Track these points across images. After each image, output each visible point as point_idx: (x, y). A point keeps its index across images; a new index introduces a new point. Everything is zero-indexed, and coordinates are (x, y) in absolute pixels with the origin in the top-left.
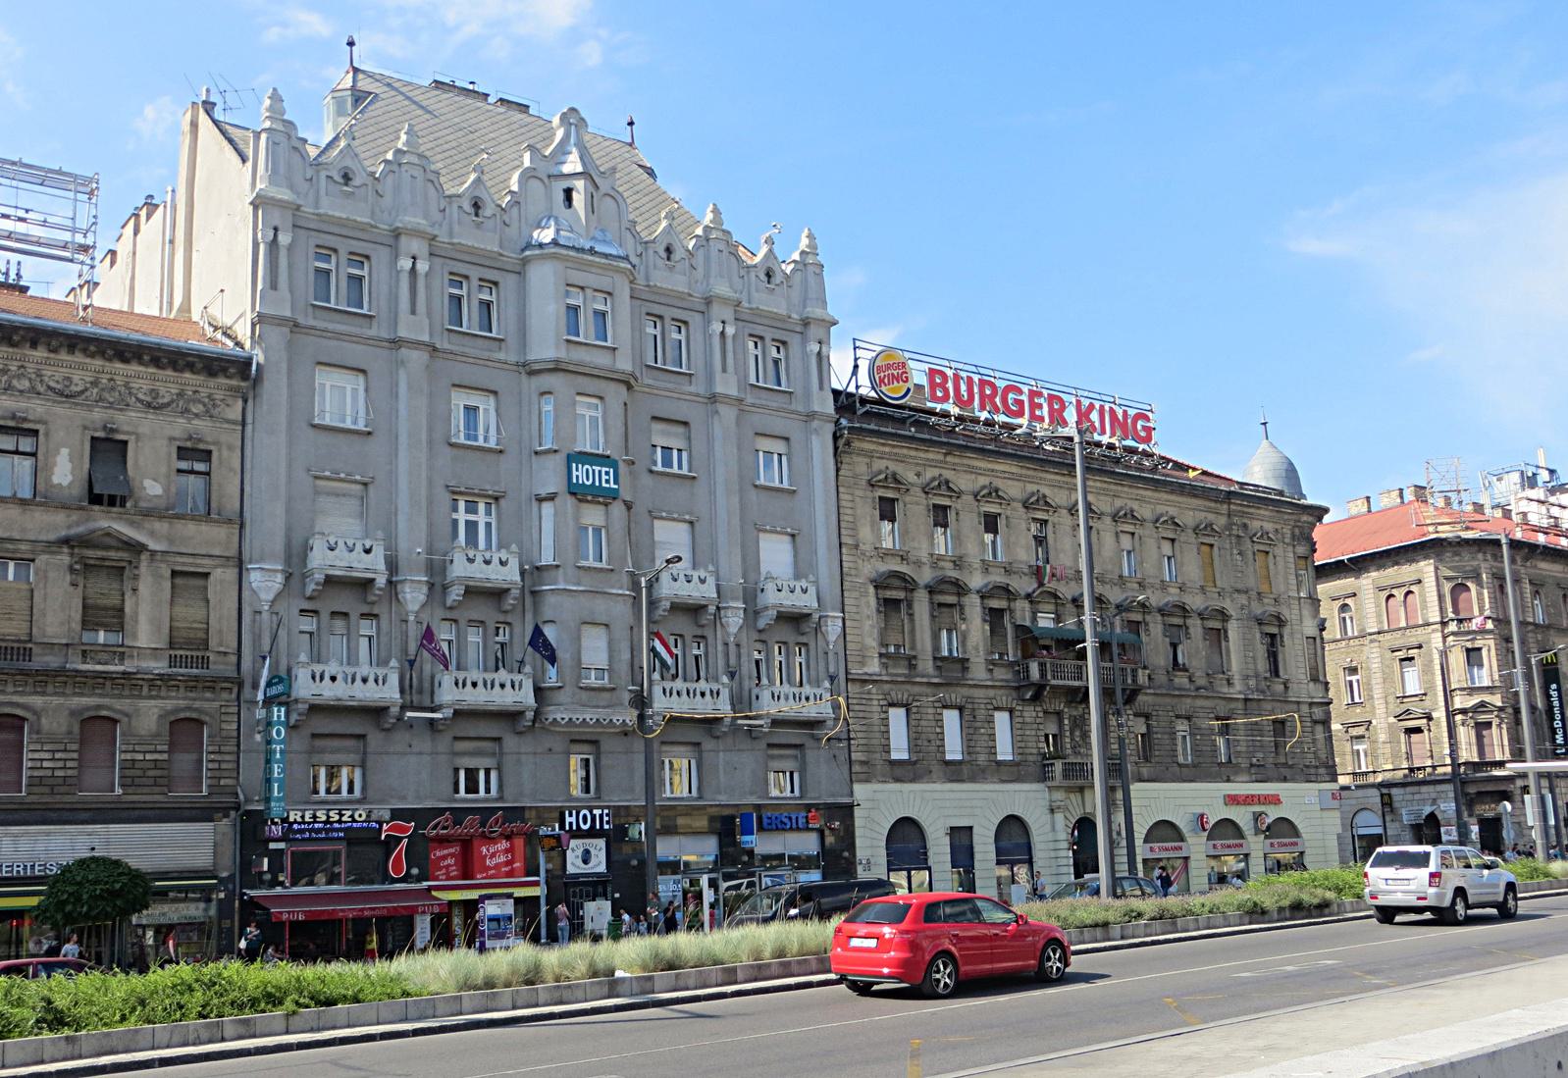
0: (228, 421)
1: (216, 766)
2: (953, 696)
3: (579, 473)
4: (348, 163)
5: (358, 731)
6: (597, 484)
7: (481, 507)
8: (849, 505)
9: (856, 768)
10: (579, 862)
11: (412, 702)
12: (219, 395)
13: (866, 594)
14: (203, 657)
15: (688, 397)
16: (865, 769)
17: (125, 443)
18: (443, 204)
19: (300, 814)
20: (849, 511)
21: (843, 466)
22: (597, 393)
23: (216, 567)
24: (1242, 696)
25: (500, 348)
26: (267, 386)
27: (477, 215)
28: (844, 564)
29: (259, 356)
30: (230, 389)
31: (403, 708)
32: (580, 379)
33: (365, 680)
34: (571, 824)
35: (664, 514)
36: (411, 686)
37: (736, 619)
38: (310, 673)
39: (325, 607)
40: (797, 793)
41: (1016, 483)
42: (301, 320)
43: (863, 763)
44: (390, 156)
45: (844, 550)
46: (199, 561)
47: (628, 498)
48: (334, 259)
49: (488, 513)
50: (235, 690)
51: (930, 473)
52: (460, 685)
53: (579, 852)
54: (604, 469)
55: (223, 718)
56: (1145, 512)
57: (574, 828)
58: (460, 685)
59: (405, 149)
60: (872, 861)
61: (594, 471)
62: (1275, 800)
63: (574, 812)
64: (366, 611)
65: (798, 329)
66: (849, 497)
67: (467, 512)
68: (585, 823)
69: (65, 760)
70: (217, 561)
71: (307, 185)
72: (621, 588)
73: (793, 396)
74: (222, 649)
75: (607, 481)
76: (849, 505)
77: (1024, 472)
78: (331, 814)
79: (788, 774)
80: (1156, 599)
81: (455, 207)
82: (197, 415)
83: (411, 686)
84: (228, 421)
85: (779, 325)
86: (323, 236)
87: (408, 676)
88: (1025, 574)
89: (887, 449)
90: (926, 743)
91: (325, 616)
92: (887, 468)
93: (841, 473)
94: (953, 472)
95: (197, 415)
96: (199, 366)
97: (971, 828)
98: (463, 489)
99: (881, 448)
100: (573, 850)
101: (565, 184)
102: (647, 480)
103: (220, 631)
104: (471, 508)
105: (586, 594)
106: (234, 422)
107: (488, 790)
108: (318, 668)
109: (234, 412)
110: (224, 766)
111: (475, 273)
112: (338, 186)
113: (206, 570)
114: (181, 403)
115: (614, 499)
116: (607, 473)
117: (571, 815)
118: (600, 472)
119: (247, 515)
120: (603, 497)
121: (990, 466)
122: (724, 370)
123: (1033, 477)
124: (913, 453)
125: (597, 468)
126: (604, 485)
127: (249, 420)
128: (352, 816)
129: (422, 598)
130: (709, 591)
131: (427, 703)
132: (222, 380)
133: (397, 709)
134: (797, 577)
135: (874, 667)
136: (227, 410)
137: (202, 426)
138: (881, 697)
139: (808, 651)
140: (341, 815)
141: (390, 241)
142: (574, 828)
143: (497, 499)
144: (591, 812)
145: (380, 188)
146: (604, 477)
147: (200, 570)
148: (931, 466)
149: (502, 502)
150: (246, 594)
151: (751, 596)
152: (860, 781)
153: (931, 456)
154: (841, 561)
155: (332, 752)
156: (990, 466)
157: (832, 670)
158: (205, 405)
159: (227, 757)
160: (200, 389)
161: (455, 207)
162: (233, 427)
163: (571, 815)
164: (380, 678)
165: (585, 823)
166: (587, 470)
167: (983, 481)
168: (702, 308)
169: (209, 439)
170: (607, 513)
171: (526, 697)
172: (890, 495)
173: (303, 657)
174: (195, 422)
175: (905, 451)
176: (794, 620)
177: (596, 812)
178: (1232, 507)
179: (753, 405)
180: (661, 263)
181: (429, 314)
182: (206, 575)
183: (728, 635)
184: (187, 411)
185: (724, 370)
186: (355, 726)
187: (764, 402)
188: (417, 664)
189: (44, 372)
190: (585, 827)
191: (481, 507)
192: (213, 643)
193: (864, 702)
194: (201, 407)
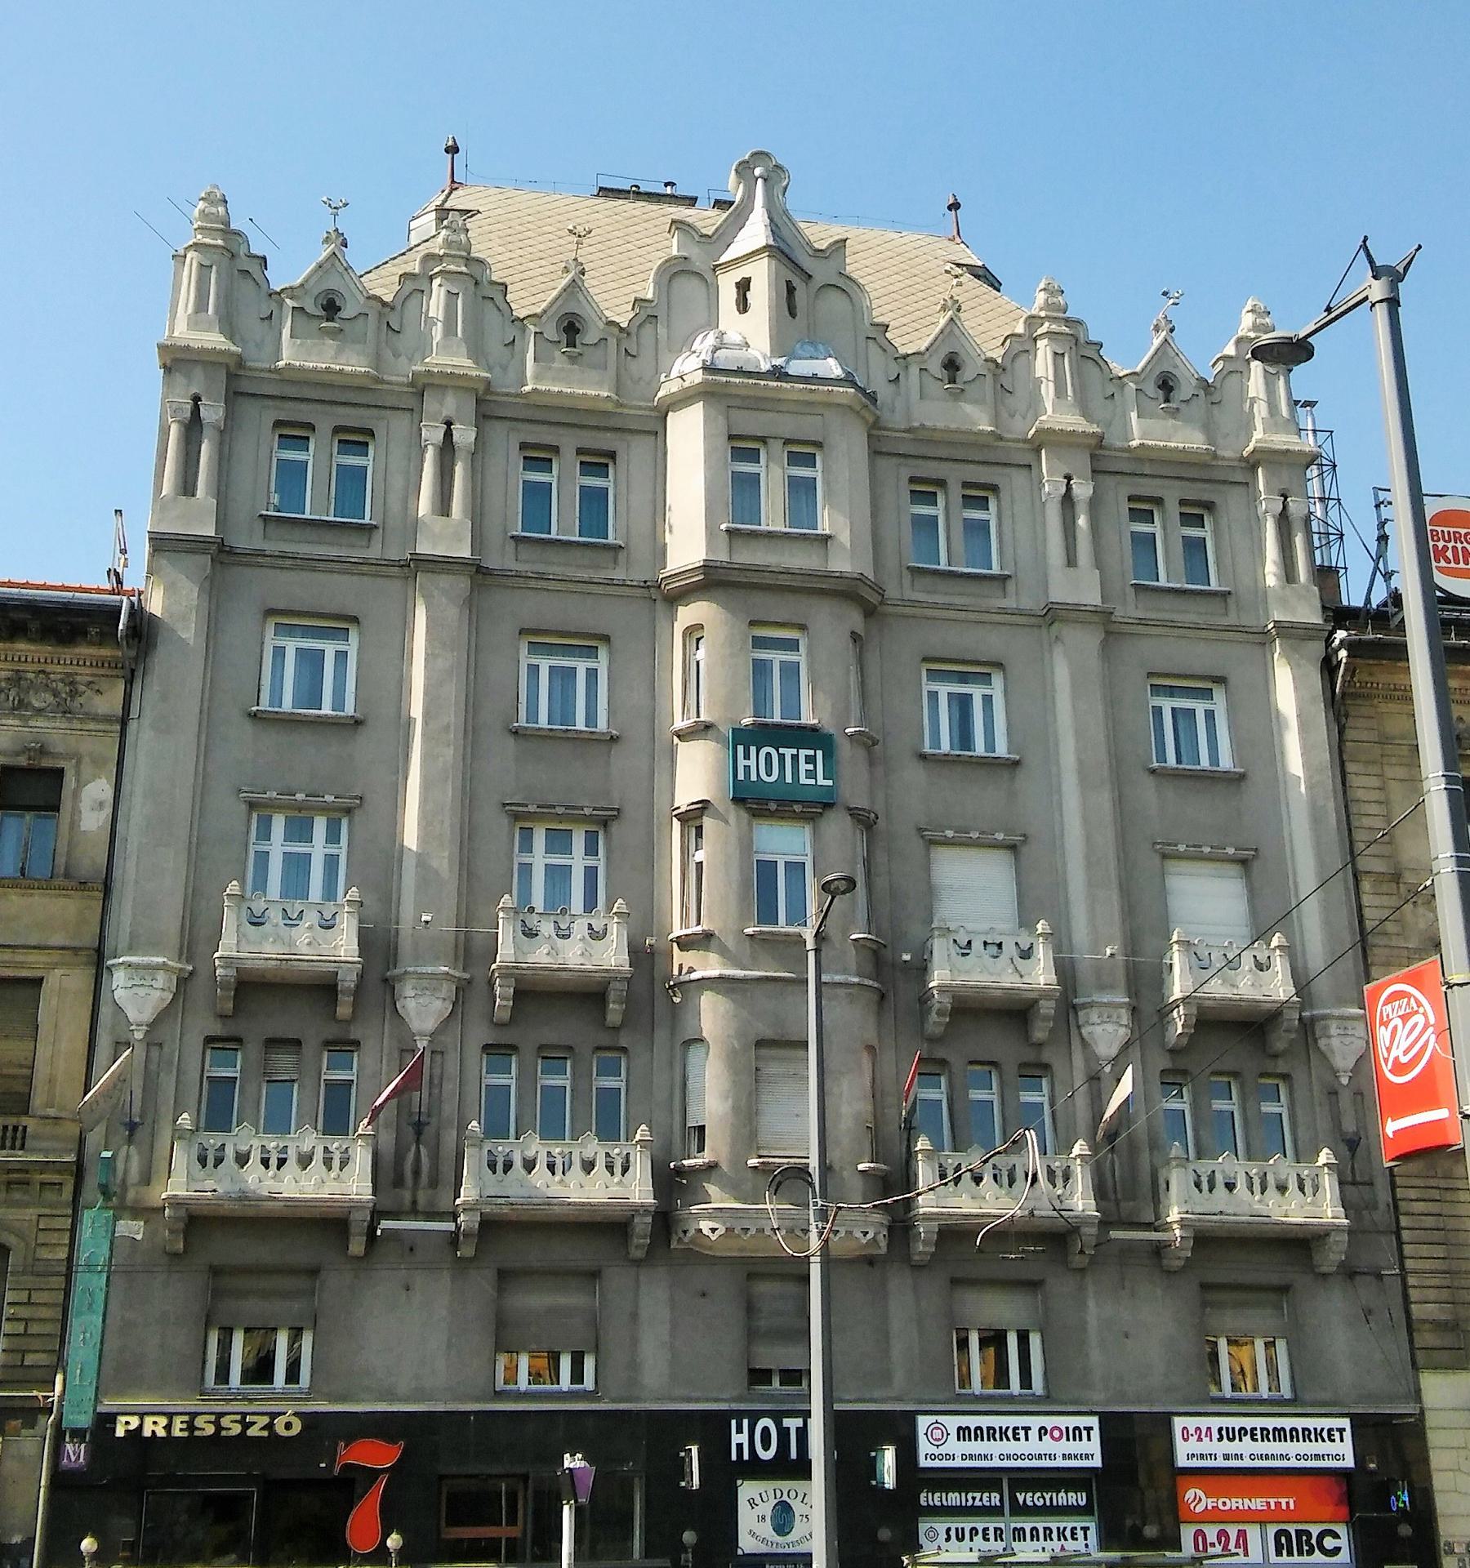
0: (95, 718)
1: (21, 1329)
3: (752, 763)
4: (333, 283)
5: (1274, 1279)
6: (789, 779)
7: (320, 826)
8: (1375, 795)
9: (1426, 1338)
10: (767, 1530)
11: (414, 1203)
12: (84, 674)
14: (15, 1129)
15: (998, 618)
16: (1448, 1340)
17: (59, 773)
18: (511, 332)
19: (163, 1421)
20: (1374, 809)
21: (1351, 722)
22: (795, 620)
23: (54, 966)
25: (615, 561)
26: (162, 659)
27: (571, 344)
28: (1367, 912)
29: (155, 605)
30: (101, 663)
31: (1105, 1224)
32: (758, 598)
33: (1282, 1188)
34: (740, 1446)
35: (950, 833)
36: (417, 1173)
37: (1110, 1028)
38: (1192, 1178)
39: (257, 1029)
40: (589, 1383)
42: (492, 562)
43: (1438, 1326)
44: (1230, 350)
45: (1366, 885)
46: (19, 958)
47: (861, 802)
48: (992, 505)
49: (333, 837)
50: (68, 1189)
52: (1205, 1186)
53: (767, 1509)
54: (803, 753)
55: (42, 1238)
57: (746, 1457)
58: (1205, 1186)
59: (1043, 314)
61: (782, 757)
63: (746, 1422)
64: (606, 1042)
65: (1239, 478)
66: (1374, 782)
67: (288, 838)
68: (766, 1446)
69: (27, 1321)
70: (56, 956)
71: (892, 387)
72: (845, 971)
73: (1231, 601)
74: (51, 1112)
75: (811, 774)
76: (1375, 795)
78: (225, 1422)
79: (1012, 1341)
81: (914, 370)
82: (39, 712)
83: (417, 1173)
84: (95, 718)
86: (341, 410)
87: (411, 1156)
91: (254, 1048)
93: (1350, 734)
95: (39, 712)
96: (34, 626)
98: (532, 808)
100: (752, 1503)
101: (737, 275)
102: (913, 775)
103: (51, 1081)
104: (300, 830)
105: (770, 986)
106: (107, 719)
107: (1026, 1381)
108: (213, 1140)
109: (110, 701)
110: (34, 1329)
111: (569, 442)
112: (315, 324)
113: (38, 974)
114: (12, 693)
115: (828, 806)
116: (811, 760)
117: (740, 1430)
118: (795, 758)
119: (117, 873)
120: (808, 808)
122: (1071, 561)
125: (789, 752)
126: (803, 780)
127: (134, 714)
128: (270, 1427)
129: (1123, 1033)
130: (1041, 974)
131: (1148, 1217)
132: (84, 651)
133: (1094, 1231)
134: (1026, 922)
136: (98, 699)
137: (53, 731)
139: (1291, 1093)
140: (246, 1426)
141: (411, 402)
142: (746, 1457)
143: (348, 811)
144: (779, 1425)
145: (1006, 381)
146: (803, 767)
147: (24, 973)
149: (615, 827)
150: (105, 1011)
151: (1143, 982)
152: (1434, 1368)
154: (1360, 908)
155: (265, 1295)
157: (1349, 1126)
158: (56, 694)
159: (44, 1313)
160: (49, 668)
161: (914, 370)
162: (108, 728)
163: (740, 1430)
164: (1204, 1179)
165: (766, 1446)
166: (768, 755)
168: (411, 402)
169: (60, 749)
170: (816, 834)
171: (638, 1189)
173: (185, 1120)
174: (40, 722)
176: (1247, 1027)
177: (787, 1422)
179: (1142, 622)
180: (936, 389)
181: (1099, 563)
182: (38, 982)
183: (1335, 1073)
184: (22, 704)
185: (1071, 561)
186: (300, 1253)
187: (1167, 616)
188: (429, 1131)
189: (78, 678)
190: (767, 1455)
191: (320, 826)
192: (37, 1101)
193: (1435, 1194)
194: (50, 698)
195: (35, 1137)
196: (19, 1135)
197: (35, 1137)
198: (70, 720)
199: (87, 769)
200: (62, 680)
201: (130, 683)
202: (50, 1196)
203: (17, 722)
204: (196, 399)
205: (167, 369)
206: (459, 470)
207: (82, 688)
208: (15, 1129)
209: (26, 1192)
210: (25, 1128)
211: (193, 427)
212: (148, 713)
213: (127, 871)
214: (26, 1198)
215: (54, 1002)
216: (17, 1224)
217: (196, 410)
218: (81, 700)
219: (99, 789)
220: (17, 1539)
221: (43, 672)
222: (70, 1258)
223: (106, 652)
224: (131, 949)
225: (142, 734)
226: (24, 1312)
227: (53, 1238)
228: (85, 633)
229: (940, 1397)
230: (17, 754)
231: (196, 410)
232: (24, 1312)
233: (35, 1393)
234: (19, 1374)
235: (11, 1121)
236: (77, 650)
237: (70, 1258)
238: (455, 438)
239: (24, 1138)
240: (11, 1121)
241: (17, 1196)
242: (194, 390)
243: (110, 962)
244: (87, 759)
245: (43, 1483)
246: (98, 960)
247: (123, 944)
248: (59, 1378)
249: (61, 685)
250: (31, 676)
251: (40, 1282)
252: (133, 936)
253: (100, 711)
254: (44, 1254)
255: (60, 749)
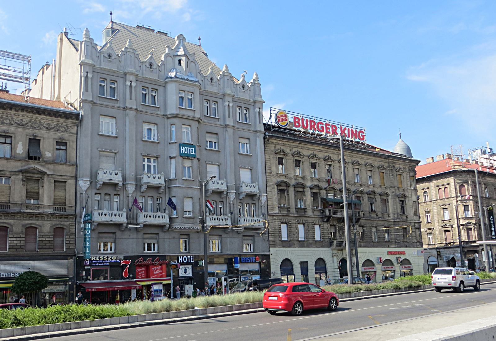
0: (72, 133)
1: (68, 242)
2: (302, 220)
3: (183, 150)
4: (110, 51)
5: (113, 231)
6: (189, 153)
7: (152, 160)
8: (269, 160)
9: (271, 243)
10: (183, 273)
11: (130, 222)
12: (69, 125)
13: (274, 188)
14: (64, 208)
15: (218, 126)
16: (274, 243)
17: (40, 140)
18: (140, 64)
19: (95, 257)
20: (269, 162)
21: (267, 147)
22: (189, 124)
23: (68, 179)
24: (393, 220)
25: (158, 110)
26: (85, 122)
27: (151, 68)
28: (267, 178)
29: (82, 113)
30: (73, 123)
31: (128, 224)
32: (184, 120)
33: (115, 215)
34: (181, 261)
35: (210, 163)
36: (130, 217)
37: (233, 196)
38: (98, 213)
39: (103, 192)
40: (252, 251)
41: (321, 153)
42: (95, 101)
43: (273, 241)
44: (123, 49)
45: (267, 174)
46: (63, 178)
47: (199, 158)
48: (106, 82)
49: (154, 162)
50: (74, 218)
51: (294, 150)
52: (146, 217)
53: (183, 270)
54: (191, 148)
55: (71, 227)
56: (362, 162)
57: (182, 262)
58: (146, 217)
59: (128, 47)
60: (276, 272)
61: (188, 149)
62: (403, 253)
63: (182, 257)
64: (116, 193)
65: (252, 104)
66: (269, 157)
67: (148, 162)
68: (185, 260)
69: (21, 240)
70: (69, 178)
71: (97, 59)
72: (196, 186)
73: (251, 125)
74: (70, 205)
75: (192, 152)
76: (269, 160)
77: (324, 149)
78: (105, 257)
79: (249, 245)
80: (366, 190)
81: (144, 65)
82: (62, 131)
83: (130, 217)
84: (72, 133)
85: (247, 103)
86: (102, 74)
87: (129, 214)
88: (324, 182)
89: (281, 142)
90: (293, 235)
91: (103, 195)
92: (281, 148)
93: (266, 150)
94: (301, 149)
95: (62, 131)
96: (63, 116)
97: (307, 262)
98: (146, 155)
99: (279, 142)
100: (181, 269)
101: (179, 58)
102: (205, 152)
103: (70, 200)
104: (149, 161)
105: (185, 188)
106: (74, 134)
107: (154, 250)
108: (101, 211)
109: (74, 130)
110: (71, 242)
111: (150, 86)
112: (107, 59)
113: (65, 180)
114: (57, 128)
115: (194, 158)
116: (192, 150)
117: (180, 258)
118: (190, 149)
119: (78, 163)
120: (191, 157)
121: (313, 147)
122: (229, 117)
123: (327, 151)
124: (289, 143)
125: (189, 148)
126: (191, 153)
127: (79, 133)
128: (111, 258)
129: (134, 189)
130: (224, 187)
131: (135, 222)
132: (70, 120)
133: (126, 224)
134: (252, 182)
135: (276, 211)
136: (72, 130)
137: (64, 135)
138: (279, 220)
139: (256, 206)
140: (108, 258)
141: (124, 76)
142: (182, 262)
143: (157, 158)
144: (187, 257)
145: (120, 59)
146: (191, 151)
147: (63, 180)
148: (294, 147)
149: (159, 159)
150: (78, 188)
151: (237, 188)
152: (272, 247)
153: (294, 144)
154: (266, 178)
155: (105, 238)
156: (313, 147)
157: (263, 212)
158: (65, 128)
159: (72, 240)
160: (63, 123)
161: (144, 65)
162: (74, 135)
163: (180, 258)
164: (120, 215)
165: (185, 260)
166: (186, 149)
167: (311, 152)
168: (222, 97)
169: (66, 139)
170: (192, 162)
171: (166, 220)
172: (282, 156)
173: (96, 208)
174: (62, 133)
175: (286, 143)
176: (251, 196)
177: (188, 257)
178: (390, 160)
179: (238, 128)
180: (209, 83)
181: (136, 99)
182: (65, 182)
183: (230, 201)
184: (59, 130)
185: (229, 117)
186: (112, 230)
187: (242, 127)
188: (132, 210)
189: (14, 118)
190: (185, 262)
191: (152, 160)
192: (67, 203)
193: (273, 222)
194: (63, 129)
229: (199, 252)
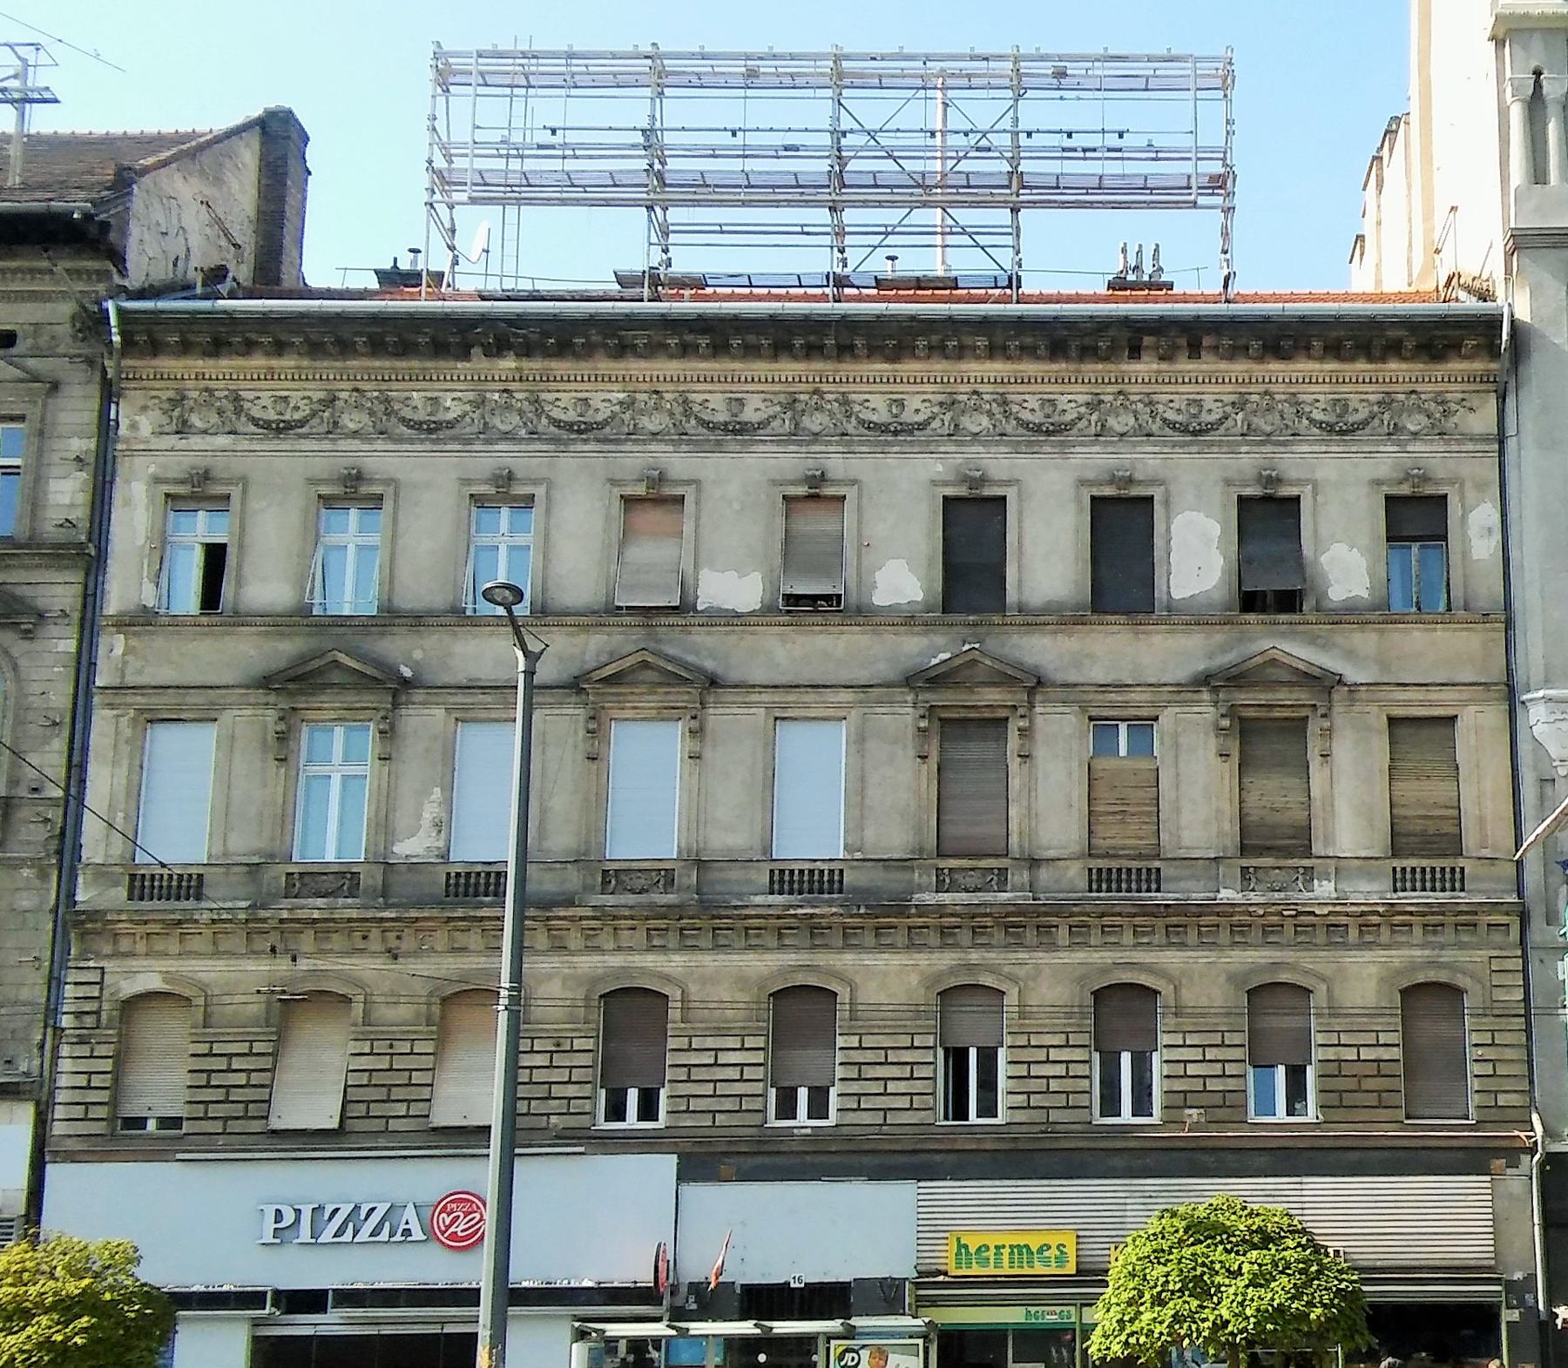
12: (1454, 392)
17: (1296, 500)
23: (1465, 703)
29: (1523, 314)
70: (1466, 693)
96: (1410, 344)
103: (1481, 820)
106: (1485, 439)
109: (1483, 419)
113: (1450, 712)
119: (1517, 605)
127: (1511, 430)
132: (1456, 366)
137: (1432, 457)
150: (1524, 748)
159: (1509, 1054)
192: (1470, 841)
194: (1425, 421)
195: (1475, 878)
196: (1458, 876)
197: (1475, 878)
198: (1447, 442)
199: (1471, 495)
200: (675, 400)
201: (1502, 398)
202: (1497, 937)
203: (1396, 449)
204: (1538, 73)
205: (1498, 41)
206: (1553, 130)
207: (1454, 407)
208: (1453, 870)
209: (1474, 933)
210: (1462, 869)
211: (1535, 104)
212: (1529, 427)
213: (1528, 597)
214: (1474, 939)
215: (1473, 742)
216: (1470, 966)
217: (1538, 85)
218: (1455, 419)
219: (1485, 515)
220: (1518, 1276)
221: (1413, 392)
222: (1526, 999)
223: (1478, 366)
224: (1547, 683)
225: (1526, 457)
226: (1490, 1053)
227: (1507, 980)
228: (1308, 348)
230: (182, 482)
231: (1538, 85)
232: (1490, 1053)
233: (1516, 1133)
234: (1493, 1115)
235: (1447, 863)
236: (1450, 365)
237: (1526, 999)
238: (1545, 91)
239: (1462, 880)
240: (1447, 863)
241: (1465, 938)
242: (1533, 64)
243: (1524, 697)
244: (1468, 485)
245: (1536, 1220)
246: (1510, 695)
247: (1537, 674)
248: (1535, 1118)
249: (1140, 406)
250: (1255, 398)
251: (1503, 1023)
252: (1547, 668)
253: (1476, 431)
254: (1500, 995)
255: (1440, 474)
